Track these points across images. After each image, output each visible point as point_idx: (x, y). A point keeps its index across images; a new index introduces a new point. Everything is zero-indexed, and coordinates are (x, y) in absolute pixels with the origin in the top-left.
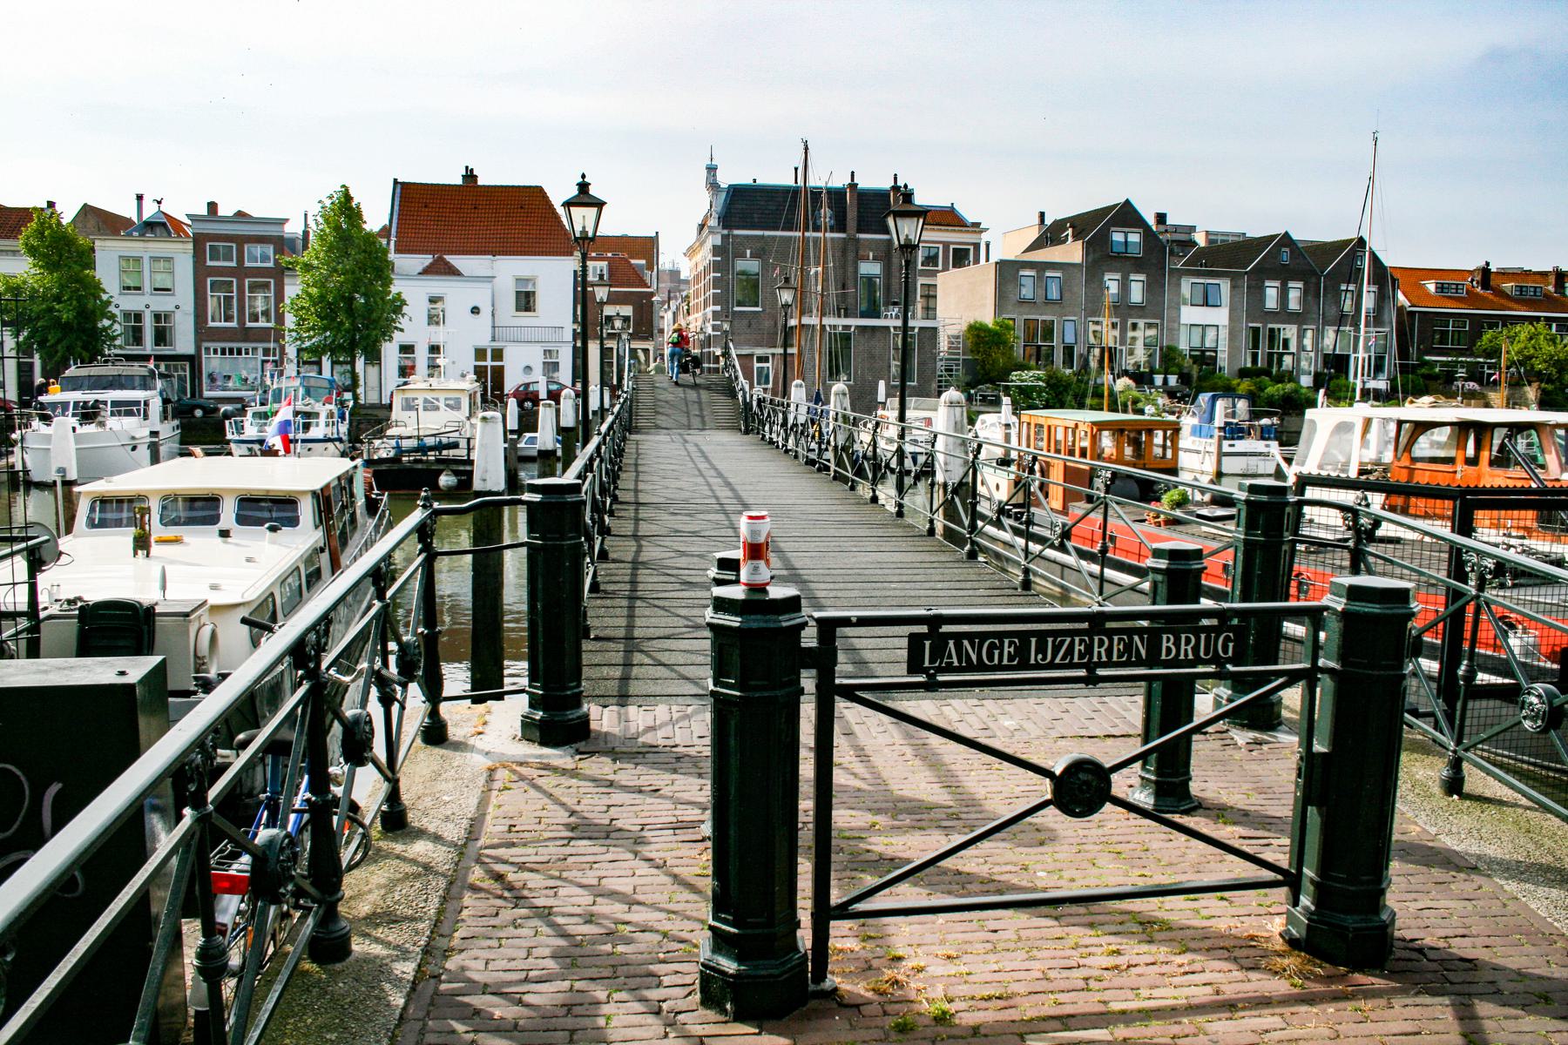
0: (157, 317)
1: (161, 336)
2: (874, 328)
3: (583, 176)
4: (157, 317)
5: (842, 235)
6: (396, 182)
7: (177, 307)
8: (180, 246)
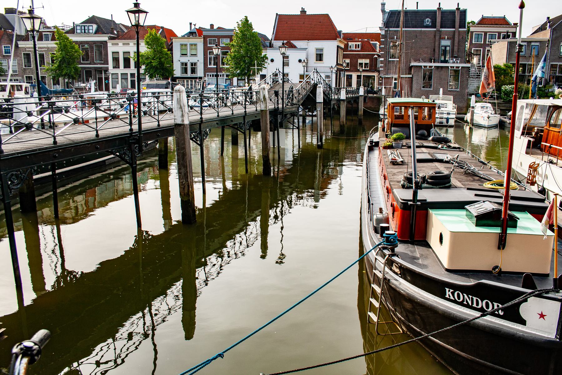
0: (192, 64)
1: (193, 71)
2: (442, 67)
4: (192, 64)
5: (454, 29)
6: (277, 14)
7: (198, 61)
8: (199, 40)
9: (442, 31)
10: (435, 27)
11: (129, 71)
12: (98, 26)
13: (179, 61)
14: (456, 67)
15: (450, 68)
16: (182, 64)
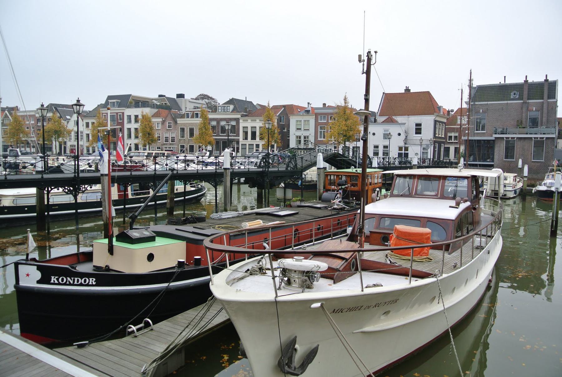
0: (305, 137)
3: (78, 98)
5: (522, 101)
6: (384, 93)
7: (310, 134)
9: (530, 102)
10: (522, 99)
11: (254, 142)
12: (235, 107)
13: (295, 134)
14: (540, 138)
15: (533, 139)
16: (297, 137)
